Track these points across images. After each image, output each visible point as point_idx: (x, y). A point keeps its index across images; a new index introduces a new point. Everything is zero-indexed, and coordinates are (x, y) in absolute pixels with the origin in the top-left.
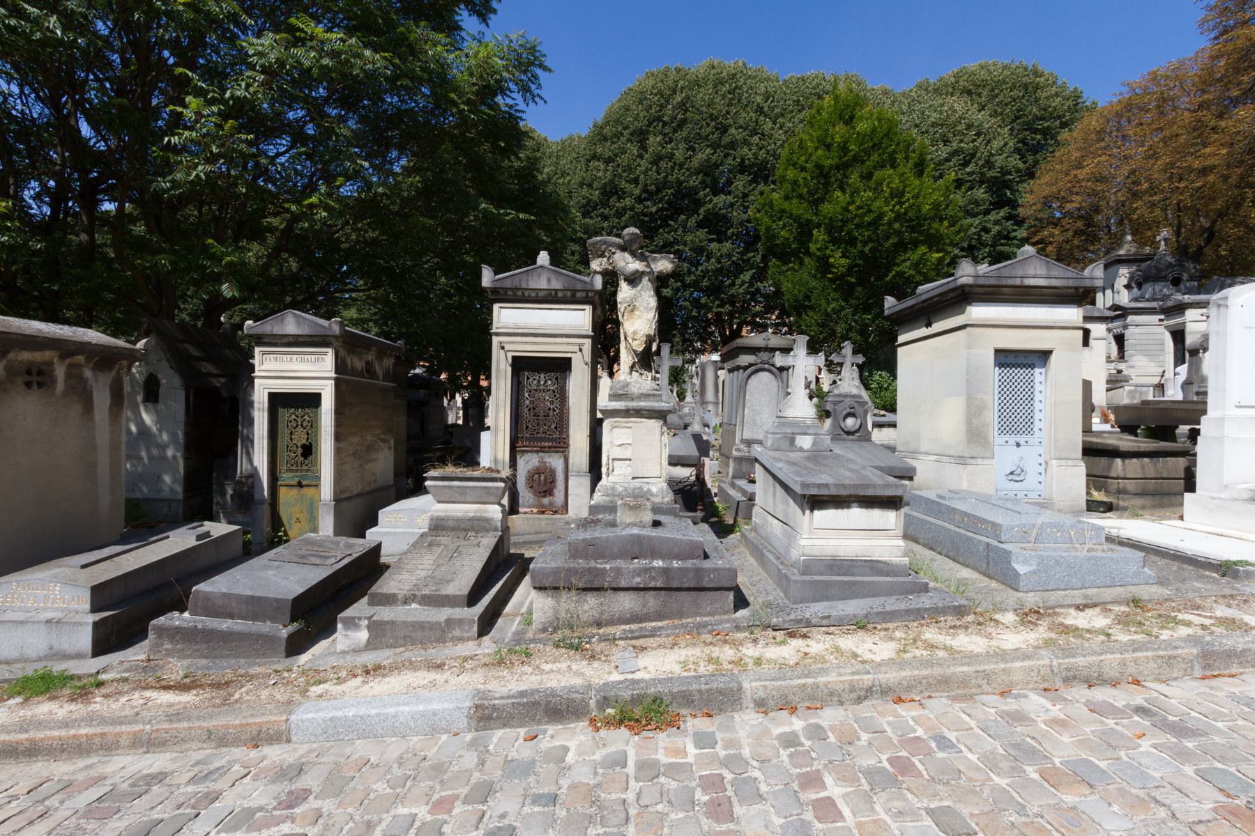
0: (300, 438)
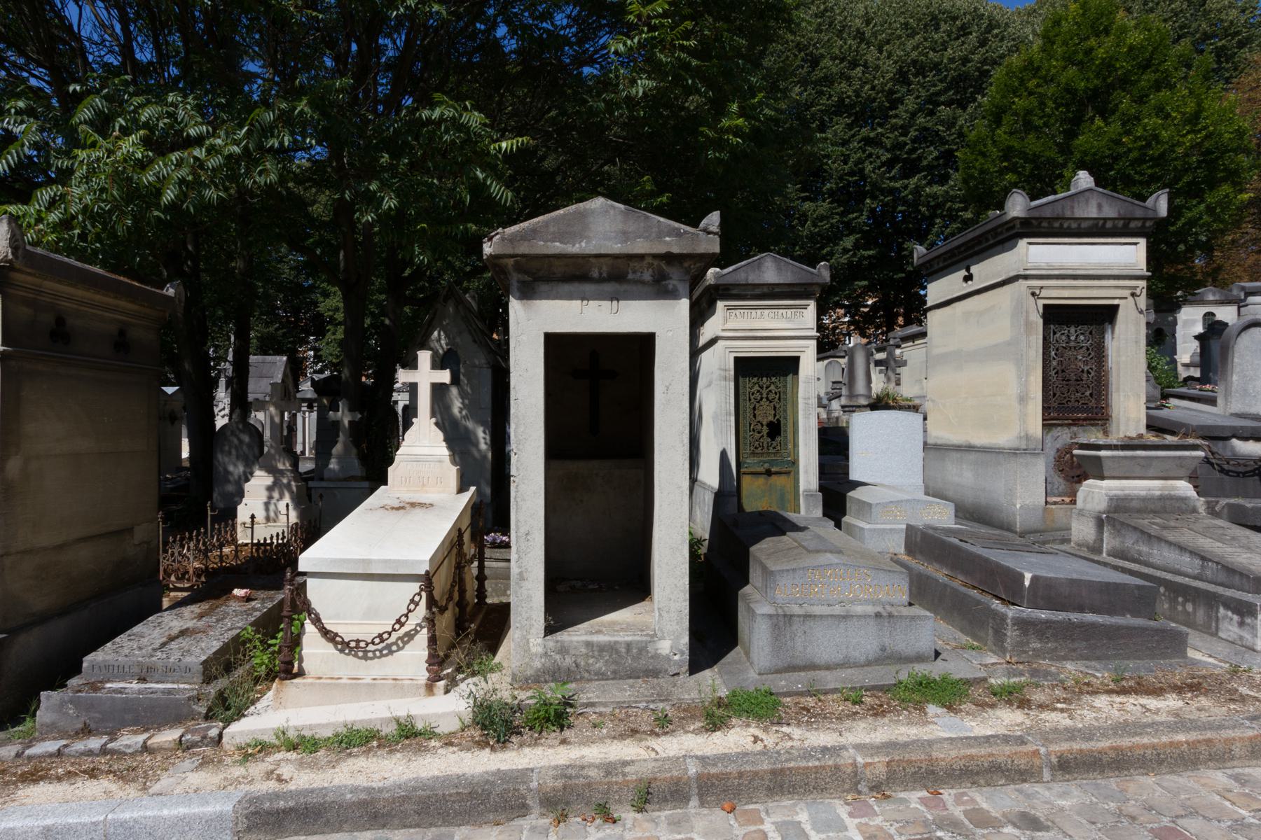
0: (766, 414)
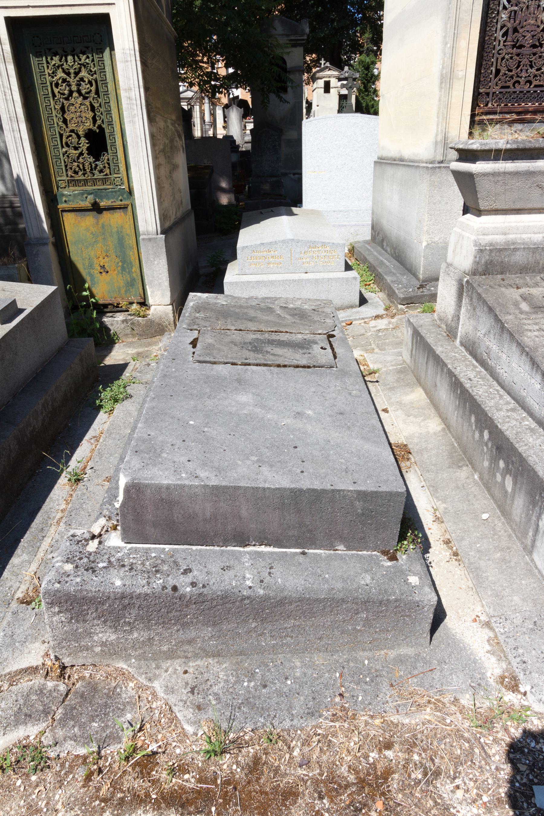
0: (81, 119)
